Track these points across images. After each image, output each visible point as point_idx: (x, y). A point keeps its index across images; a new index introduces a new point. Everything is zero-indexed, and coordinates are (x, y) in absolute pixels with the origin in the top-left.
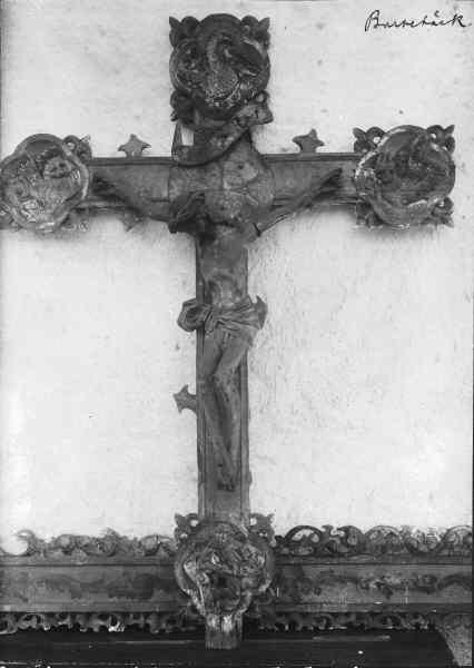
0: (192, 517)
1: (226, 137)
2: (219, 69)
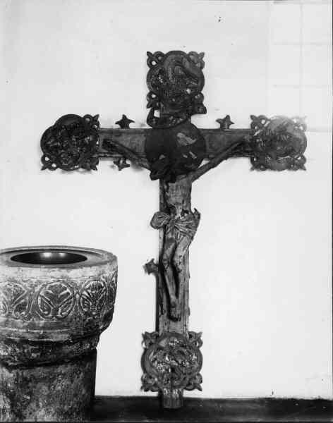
0: (98, 124)
1: (179, 118)
2: (175, 81)
